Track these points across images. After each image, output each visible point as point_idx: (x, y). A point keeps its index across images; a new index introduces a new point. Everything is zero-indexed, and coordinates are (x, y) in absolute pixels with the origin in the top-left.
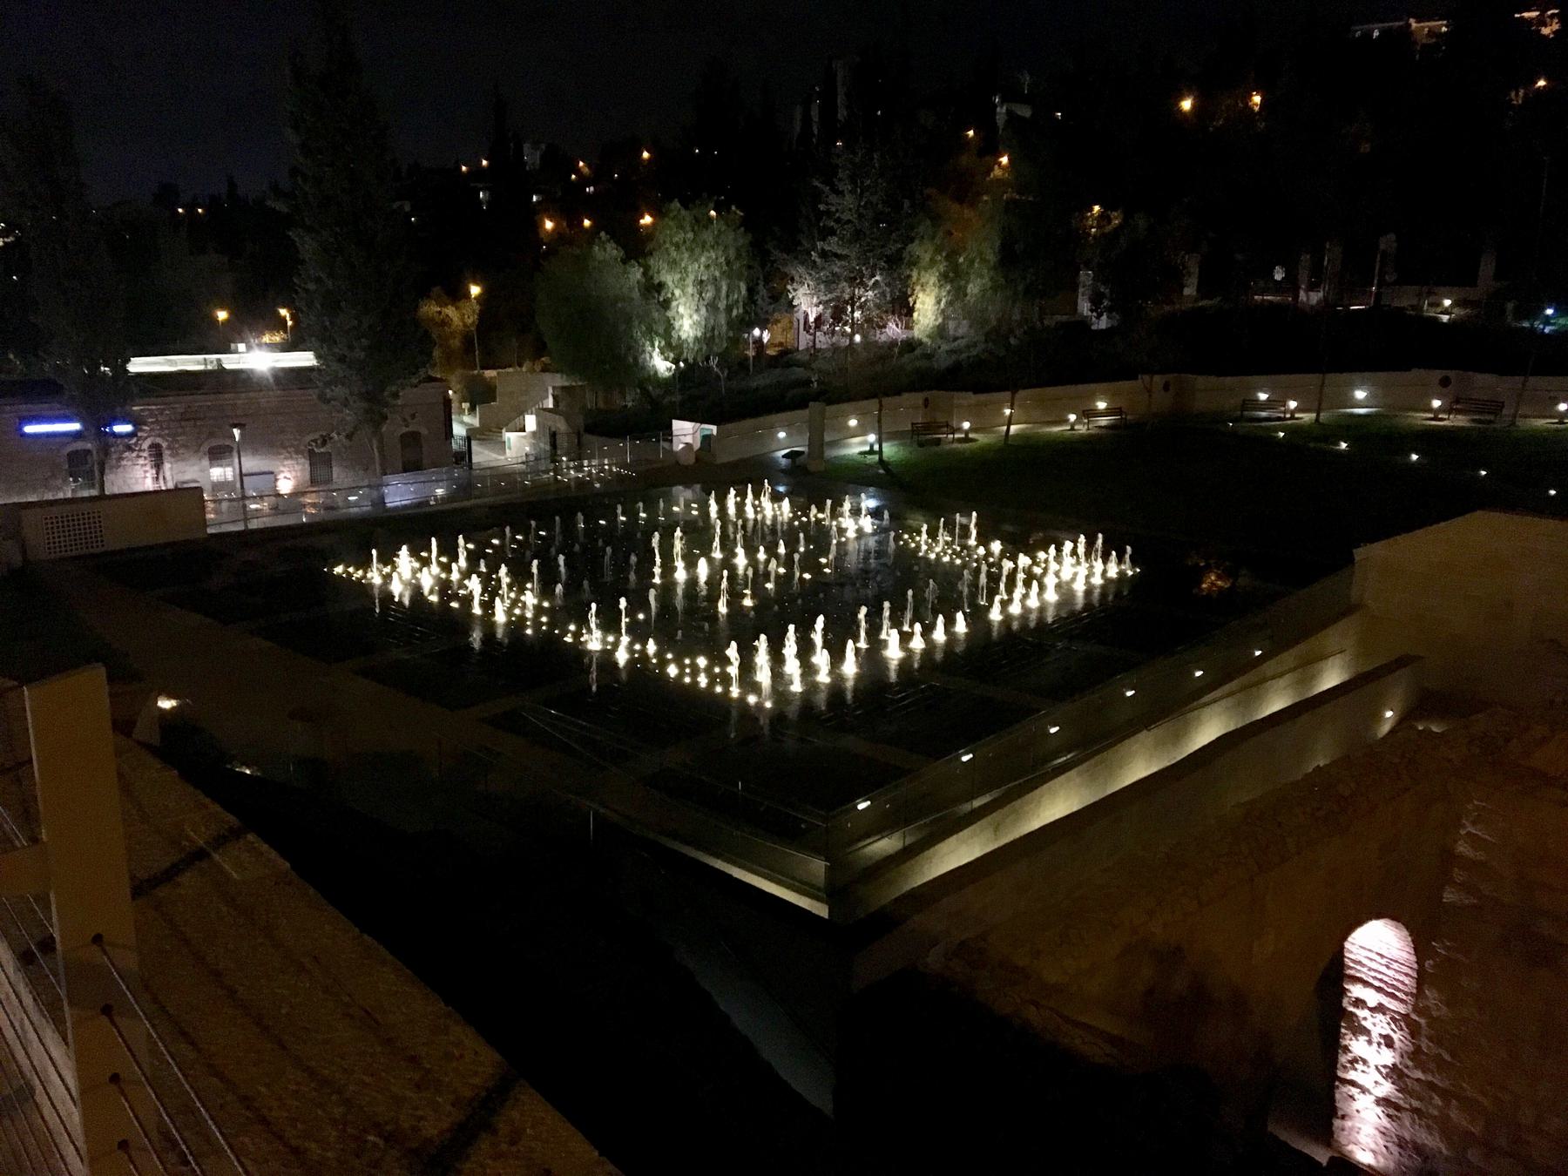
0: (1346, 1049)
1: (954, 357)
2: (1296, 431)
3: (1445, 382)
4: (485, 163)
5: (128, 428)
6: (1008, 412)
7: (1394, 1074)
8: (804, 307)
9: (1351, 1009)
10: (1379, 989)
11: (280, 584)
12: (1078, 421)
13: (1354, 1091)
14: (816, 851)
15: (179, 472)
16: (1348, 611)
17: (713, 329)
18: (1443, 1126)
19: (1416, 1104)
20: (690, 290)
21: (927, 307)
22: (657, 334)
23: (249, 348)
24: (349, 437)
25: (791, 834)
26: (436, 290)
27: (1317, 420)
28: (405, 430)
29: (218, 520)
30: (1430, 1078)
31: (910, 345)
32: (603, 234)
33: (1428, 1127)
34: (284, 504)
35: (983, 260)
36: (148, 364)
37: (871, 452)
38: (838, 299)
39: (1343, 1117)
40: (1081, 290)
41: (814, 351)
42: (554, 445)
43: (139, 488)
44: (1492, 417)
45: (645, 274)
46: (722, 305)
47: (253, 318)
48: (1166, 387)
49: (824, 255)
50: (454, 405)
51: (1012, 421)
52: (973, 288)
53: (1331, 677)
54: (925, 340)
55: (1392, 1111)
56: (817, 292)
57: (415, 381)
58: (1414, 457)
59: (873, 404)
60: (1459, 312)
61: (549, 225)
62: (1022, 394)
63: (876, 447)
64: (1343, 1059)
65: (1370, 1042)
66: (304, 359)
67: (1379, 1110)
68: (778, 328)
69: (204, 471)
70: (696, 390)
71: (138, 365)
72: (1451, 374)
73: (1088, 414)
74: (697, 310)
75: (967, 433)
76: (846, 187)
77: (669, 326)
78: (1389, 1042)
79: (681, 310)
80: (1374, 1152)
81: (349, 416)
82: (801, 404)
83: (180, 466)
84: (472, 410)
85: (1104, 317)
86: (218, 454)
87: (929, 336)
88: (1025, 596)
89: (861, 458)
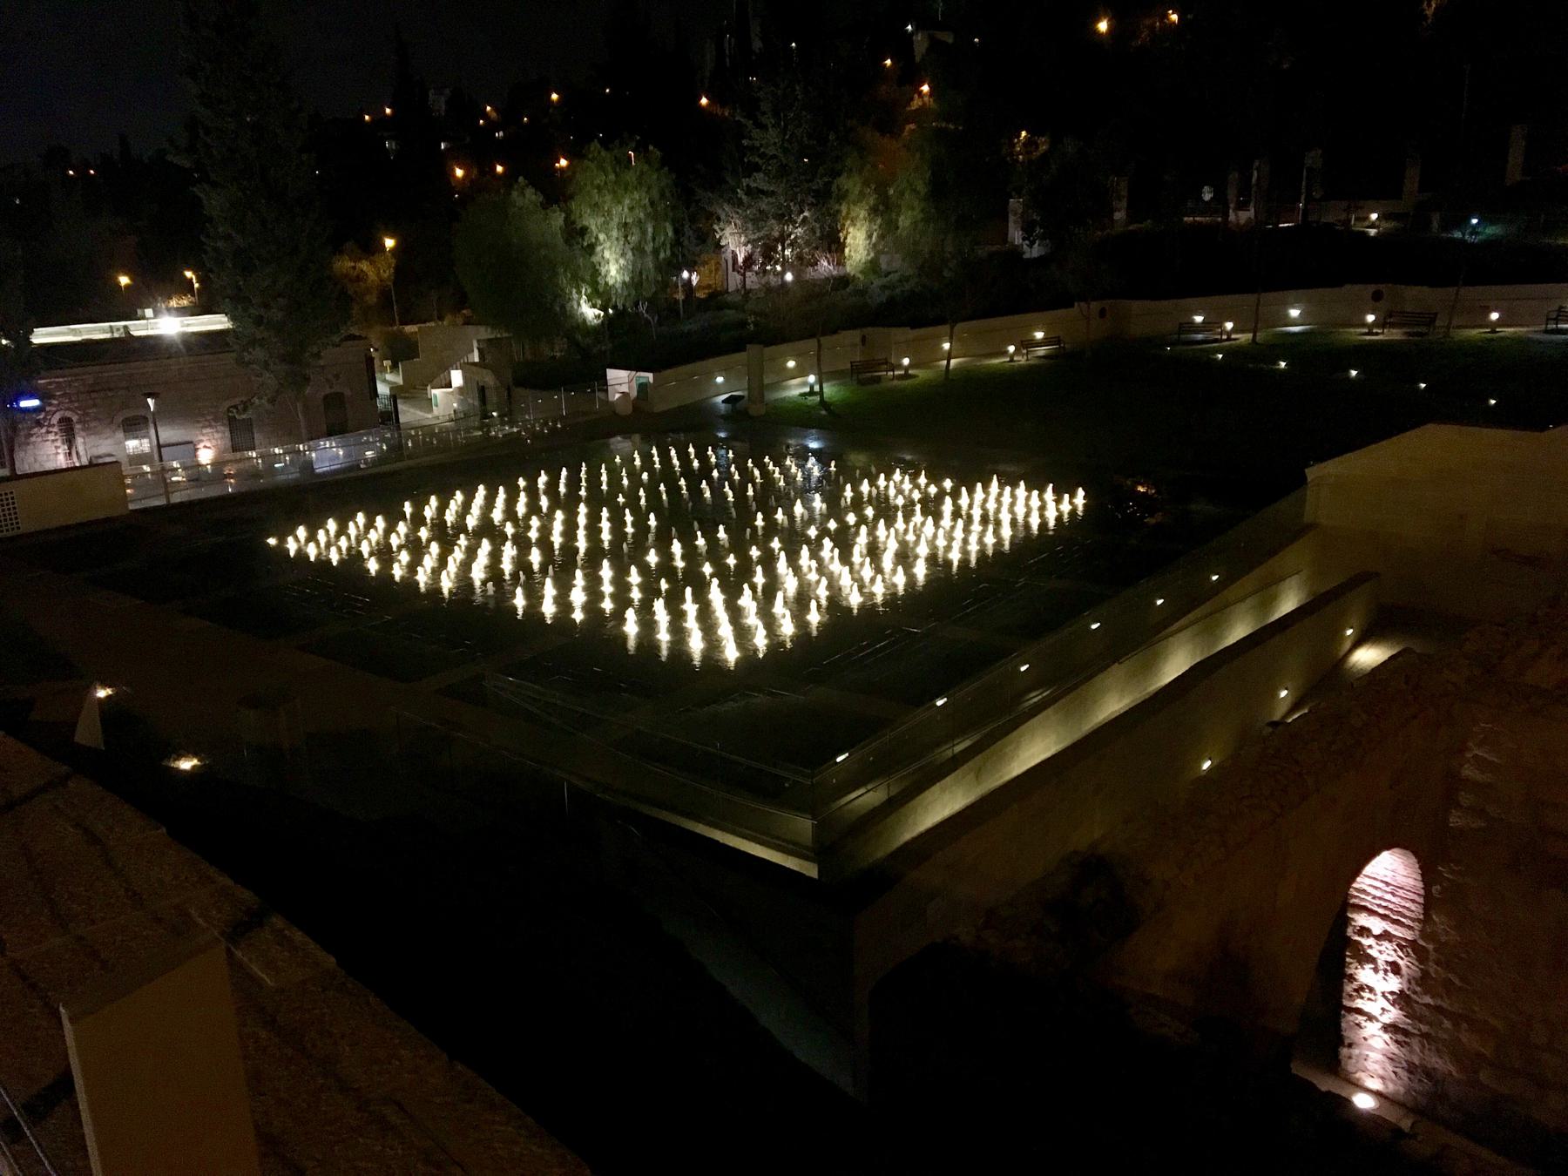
0: (1352, 978)
1: (887, 293)
2: (1234, 353)
4: (388, 111)
5: (35, 403)
6: (946, 346)
7: (1401, 999)
8: (732, 247)
9: (1356, 938)
10: (1384, 917)
11: (206, 556)
12: (1017, 351)
13: (1361, 1019)
14: (799, 809)
15: (89, 447)
16: (1297, 531)
18: (1456, 1052)
19: (1424, 1028)
20: (615, 233)
21: (858, 242)
22: (583, 281)
23: (156, 314)
24: (272, 401)
25: (773, 792)
26: (349, 245)
28: (328, 391)
29: (136, 499)
30: (1439, 1002)
31: (843, 281)
32: (521, 179)
33: (1438, 1050)
34: (197, 475)
35: (914, 190)
36: (51, 335)
37: (812, 393)
38: (768, 236)
39: (1350, 1045)
40: (1012, 218)
42: (483, 399)
43: (50, 466)
44: (1424, 330)
45: (566, 220)
46: (649, 248)
47: (159, 281)
48: (1102, 313)
49: (749, 191)
50: (377, 363)
51: (950, 353)
52: (904, 221)
53: (1288, 603)
55: (1400, 1037)
56: (745, 231)
57: (336, 339)
58: (1354, 373)
59: (812, 344)
60: (1386, 225)
61: (459, 173)
62: (959, 326)
63: (817, 388)
64: (1349, 988)
65: (1376, 970)
66: (217, 322)
67: (1386, 1037)
68: (705, 270)
69: (121, 443)
70: (626, 338)
71: (43, 336)
72: (1381, 287)
73: (1027, 344)
74: (623, 255)
75: (906, 369)
76: (768, 120)
77: (596, 272)
78: (1395, 968)
79: (607, 254)
80: (1382, 1078)
81: (269, 379)
82: (737, 346)
83: (92, 440)
84: (394, 367)
86: (134, 426)
88: (982, 534)
89: (801, 400)
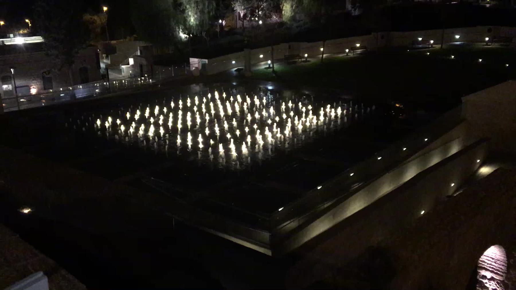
2: (434, 53)
3: (489, 31)
8: (238, 11)
10: (492, 272)
17: (203, 20)
20: (193, 5)
22: (181, 24)
23: (14, 36)
24: (60, 70)
27: (441, 47)
31: (281, 24)
34: (31, 98)
37: (269, 67)
38: (252, 7)
41: (244, 28)
42: (141, 70)
46: (206, 11)
48: (382, 37)
50: (100, 56)
53: (454, 150)
54: (289, 23)
57: (84, 46)
59: (269, 48)
62: (327, 42)
63: (271, 66)
66: (37, 39)
70: (197, 46)
75: (306, 58)
79: (190, 13)
84: (107, 57)
85: (357, 10)
87: (289, 20)
89: (265, 70)
